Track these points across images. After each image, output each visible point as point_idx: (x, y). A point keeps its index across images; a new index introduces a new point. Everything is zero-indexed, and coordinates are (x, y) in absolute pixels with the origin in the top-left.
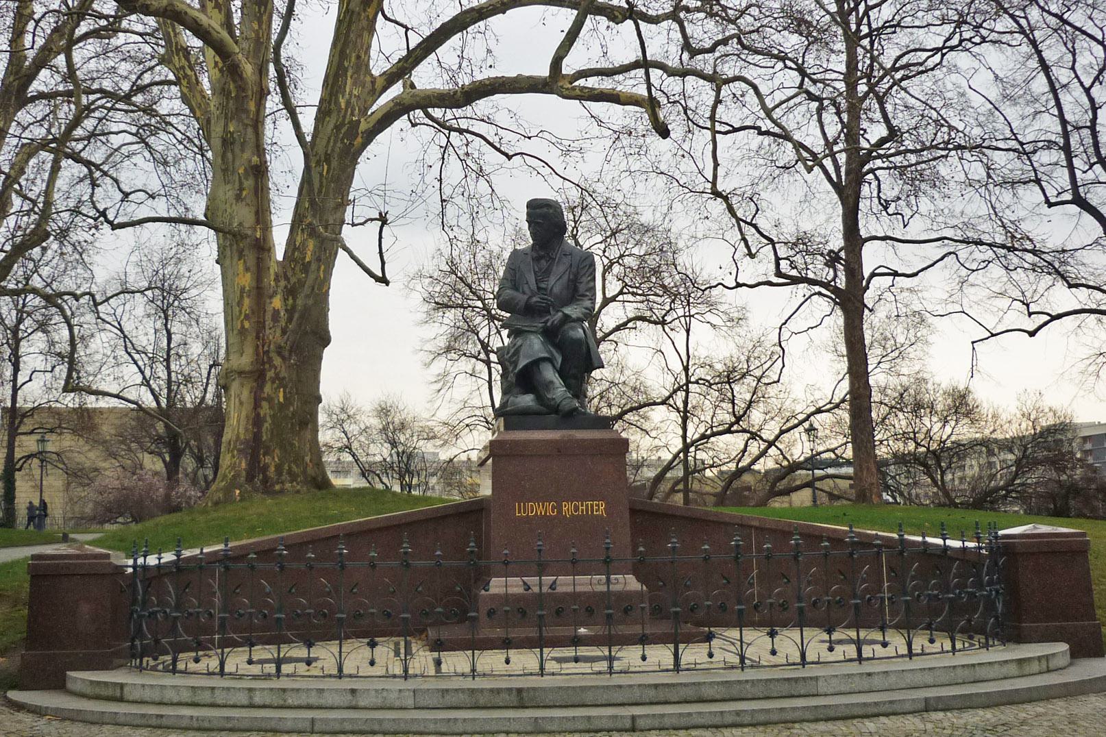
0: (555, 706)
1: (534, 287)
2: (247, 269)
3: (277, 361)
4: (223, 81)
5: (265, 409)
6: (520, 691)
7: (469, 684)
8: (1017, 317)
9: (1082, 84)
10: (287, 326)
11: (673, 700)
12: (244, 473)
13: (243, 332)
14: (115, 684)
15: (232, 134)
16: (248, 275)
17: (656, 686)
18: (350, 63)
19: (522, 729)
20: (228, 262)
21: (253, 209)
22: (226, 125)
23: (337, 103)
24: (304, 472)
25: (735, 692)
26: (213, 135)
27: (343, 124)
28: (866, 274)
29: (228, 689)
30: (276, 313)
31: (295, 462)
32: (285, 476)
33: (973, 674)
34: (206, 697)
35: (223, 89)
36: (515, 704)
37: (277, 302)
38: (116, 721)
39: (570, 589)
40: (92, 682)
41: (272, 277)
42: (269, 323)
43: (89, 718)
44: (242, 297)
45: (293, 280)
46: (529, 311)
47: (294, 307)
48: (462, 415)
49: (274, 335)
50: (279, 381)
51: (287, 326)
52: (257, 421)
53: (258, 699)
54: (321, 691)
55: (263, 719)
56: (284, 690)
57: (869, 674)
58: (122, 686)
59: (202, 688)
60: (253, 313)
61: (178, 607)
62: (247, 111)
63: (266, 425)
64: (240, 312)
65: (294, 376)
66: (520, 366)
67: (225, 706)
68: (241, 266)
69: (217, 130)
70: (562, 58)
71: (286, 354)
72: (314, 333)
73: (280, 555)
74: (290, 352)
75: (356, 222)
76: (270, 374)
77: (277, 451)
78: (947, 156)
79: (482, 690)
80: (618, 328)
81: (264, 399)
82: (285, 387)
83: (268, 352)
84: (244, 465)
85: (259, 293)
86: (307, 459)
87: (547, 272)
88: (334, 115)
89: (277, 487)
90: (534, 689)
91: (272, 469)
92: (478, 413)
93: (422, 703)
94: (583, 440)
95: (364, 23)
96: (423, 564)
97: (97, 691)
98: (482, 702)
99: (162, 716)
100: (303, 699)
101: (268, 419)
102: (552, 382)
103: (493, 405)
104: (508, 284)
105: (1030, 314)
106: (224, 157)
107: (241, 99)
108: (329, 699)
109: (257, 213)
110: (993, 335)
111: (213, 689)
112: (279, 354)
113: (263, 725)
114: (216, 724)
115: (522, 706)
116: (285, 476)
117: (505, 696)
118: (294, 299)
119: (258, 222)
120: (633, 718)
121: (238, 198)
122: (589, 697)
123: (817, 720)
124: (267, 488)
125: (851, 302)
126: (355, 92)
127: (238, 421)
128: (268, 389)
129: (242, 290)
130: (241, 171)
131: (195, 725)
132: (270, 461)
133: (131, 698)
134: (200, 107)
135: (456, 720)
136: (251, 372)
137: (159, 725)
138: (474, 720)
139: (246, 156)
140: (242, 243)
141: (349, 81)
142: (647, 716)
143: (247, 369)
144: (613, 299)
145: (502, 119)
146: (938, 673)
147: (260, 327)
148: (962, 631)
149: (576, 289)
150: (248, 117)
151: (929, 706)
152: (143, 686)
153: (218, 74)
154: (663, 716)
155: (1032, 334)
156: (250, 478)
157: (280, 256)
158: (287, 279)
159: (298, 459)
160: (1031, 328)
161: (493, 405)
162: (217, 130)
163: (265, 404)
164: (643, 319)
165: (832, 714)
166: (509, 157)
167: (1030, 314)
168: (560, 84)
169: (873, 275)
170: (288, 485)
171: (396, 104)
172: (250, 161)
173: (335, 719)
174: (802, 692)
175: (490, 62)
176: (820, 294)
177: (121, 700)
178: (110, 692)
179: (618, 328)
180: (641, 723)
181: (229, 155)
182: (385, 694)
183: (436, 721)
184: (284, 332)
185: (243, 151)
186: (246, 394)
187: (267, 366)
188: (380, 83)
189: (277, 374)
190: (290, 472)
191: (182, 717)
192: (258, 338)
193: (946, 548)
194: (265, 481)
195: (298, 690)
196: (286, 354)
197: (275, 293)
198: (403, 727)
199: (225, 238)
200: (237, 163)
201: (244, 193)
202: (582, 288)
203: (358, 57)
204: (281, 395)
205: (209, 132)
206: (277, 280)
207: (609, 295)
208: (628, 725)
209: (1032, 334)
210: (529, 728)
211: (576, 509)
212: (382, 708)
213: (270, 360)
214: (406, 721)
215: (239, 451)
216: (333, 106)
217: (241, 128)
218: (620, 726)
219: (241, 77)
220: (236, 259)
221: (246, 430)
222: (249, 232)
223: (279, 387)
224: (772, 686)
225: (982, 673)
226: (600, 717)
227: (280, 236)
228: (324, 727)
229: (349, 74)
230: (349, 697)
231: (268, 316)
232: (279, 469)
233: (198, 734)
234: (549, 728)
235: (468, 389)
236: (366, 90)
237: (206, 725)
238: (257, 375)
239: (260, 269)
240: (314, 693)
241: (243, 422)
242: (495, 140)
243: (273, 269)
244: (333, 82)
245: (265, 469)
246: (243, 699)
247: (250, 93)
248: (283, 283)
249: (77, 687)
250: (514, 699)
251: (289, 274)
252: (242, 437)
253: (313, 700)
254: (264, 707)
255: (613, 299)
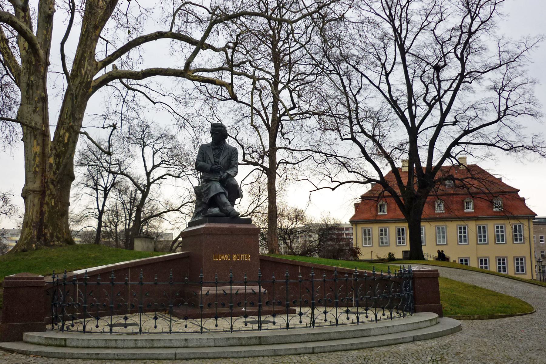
0: (274, 344)
1: (213, 162)
2: (38, 144)
3: (51, 187)
4: (28, 57)
5: (45, 208)
6: (260, 338)
7: (229, 335)
8: (327, 182)
9: (352, 93)
10: (56, 171)
11: (320, 339)
12: (36, 237)
13: (35, 173)
14: (61, 339)
15: (32, 81)
16: (39, 147)
17: (314, 334)
18: (87, 55)
19: (269, 354)
20: (28, 140)
21: (42, 117)
22: (29, 78)
23: (81, 72)
24: (63, 237)
25: (343, 335)
26: (22, 81)
27: (83, 82)
28: (277, 162)
29: (124, 340)
30: (51, 165)
31: (59, 232)
32: (55, 239)
33: (418, 326)
34: (113, 344)
35: (28, 60)
36: (258, 343)
37: (51, 160)
38: (72, 357)
39: (214, 292)
40: (46, 338)
41: (49, 149)
42: (47, 169)
43: (57, 355)
44: (35, 157)
45: (59, 150)
46: (213, 171)
47: (59, 162)
48: (85, 212)
49: (50, 175)
50: (52, 195)
51: (56, 171)
52: (42, 213)
53: (139, 345)
54: (171, 340)
55: (151, 354)
56: (153, 340)
57: (388, 327)
58: (65, 340)
59: (111, 340)
60: (40, 164)
61: (64, 302)
62: (40, 72)
63: (46, 215)
64: (35, 164)
65: (59, 194)
66: (210, 196)
67: (123, 348)
68: (35, 142)
69: (24, 79)
70: (190, 62)
71: (56, 184)
72: (68, 175)
73: (113, 278)
74: (58, 182)
75: (105, 126)
76: (48, 192)
77: (51, 227)
78: (310, 117)
79: (244, 338)
80: (159, 178)
81: (45, 204)
82: (55, 199)
83: (47, 182)
84: (35, 233)
85: (44, 155)
86: (64, 231)
87: (219, 155)
88: (79, 78)
89: (52, 243)
90: (266, 337)
91: (49, 235)
92: (92, 211)
93: (217, 344)
94: (241, 229)
95: (94, 37)
96: (173, 279)
97: (50, 342)
98: (244, 343)
99: (98, 354)
100: (162, 344)
101: (47, 212)
102: (226, 203)
103: (98, 208)
104: (200, 159)
105: (332, 182)
106: (27, 92)
107: (37, 66)
108: (175, 344)
109: (43, 119)
110: (318, 189)
111: (116, 340)
112: (53, 184)
113: (151, 357)
114: (127, 357)
115: (261, 344)
116: (55, 239)
117: (253, 340)
118: (59, 159)
119: (43, 123)
120: (313, 348)
121: (35, 111)
122: (288, 339)
123: (379, 346)
124: (46, 243)
125: (271, 173)
126: (89, 68)
127: (33, 213)
128: (47, 199)
129: (36, 154)
130: (36, 99)
131: (116, 357)
132: (48, 232)
133: (71, 345)
134: (14, 67)
135: (241, 352)
136: (39, 191)
137: (97, 358)
138: (249, 351)
139: (38, 92)
140: (34, 132)
141: (86, 63)
142: (318, 347)
143: (38, 189)
144: (158, 166)
145: (153, 86)
146: (409, 325)
147: (43, 171)
148: (396, 308)
149: (230, 163)
150: (40, 74)
151: (415, 339)
152: (78, 339)
153: (25, 53)
154: (324, 347)
155: (333, 189)
156: (39, 238)
157: (52, 140)
158: (56, 149)
159: (60, 231)
160: (333, 187)
161: (98, 208)
162: (24, 79)
163: (45, 206)
164: (170, 175)
165: (384, 343)
166: (154, 103)
167: (332, 182)
168: (189, 74)
169: (280, 163)
170: (56, 243)
171: (109, 75)
172: (41, 95)
173: (186, 353)
174: (366, 335)
175: (140, 61)
176: (258, 169)
177: (65, 346)
178: (58, 342)
179: (159, 178)
180: (316, 350)
181: (31, 91)
182: (201, 340)
183: (232, 352)
184: (55, 174)
185: (37, 90)
186: (36, 201)
187: (46, 189)
188: (100, 65)
189: (51, 193)
190: (57, 236)
191: (109, 354)
192: (42, 176)
193: (106, 265)
194: (45, 240)
195: (159, 340)
196: (56, 184)
197: (51, 156)
198: (217, 355)
199: (27, 130)
200: (34, 95)
201: (38, 109)
202: (233, 163)
203: (91, 52)
204: (53, 202)
205: (19, 80)
206: (51, 150)
207: (155, 164)
208: (311, 351)
209: (333, 189)
210: (272, 354)
211: (238, 257)
212: (199, 347)
213: (48, 186)
214: (219, 353)
215: (33, 226)
216: (78, 73)
217: (37, 79)
218: (308, 351)
219: (38, 55)
220: (33, 139)
221: (37, 217)
222: (40, 128)
223: (52, 199)
224: (356, 333)
225: (373, 333)
226: (300, 348)
227: (52, 131)
228: (181, 357)
229: (87, 59)
230: (184, 342)
231: (47, 166)
232: (52, 235)
233: (117, 362)
234: (280, 354)
235: (88, 201)
236: (94, 68)
237: (122, 357)
238: (42, 193)
239: (44, 144)
240: (167, 341)
241: (35, 214)
242: (148, 95)
243: (50, 145)
244: (79, 61)
245: (45, 235)
246: (132, 344)
247: (42, 63)
248: (54, 152)
249: (29, 339)
250: (257, 341)
251: (57, 147)
252: (34, 220)
253: (167, 345)
254: (143, 348)
255: (158, 166)
